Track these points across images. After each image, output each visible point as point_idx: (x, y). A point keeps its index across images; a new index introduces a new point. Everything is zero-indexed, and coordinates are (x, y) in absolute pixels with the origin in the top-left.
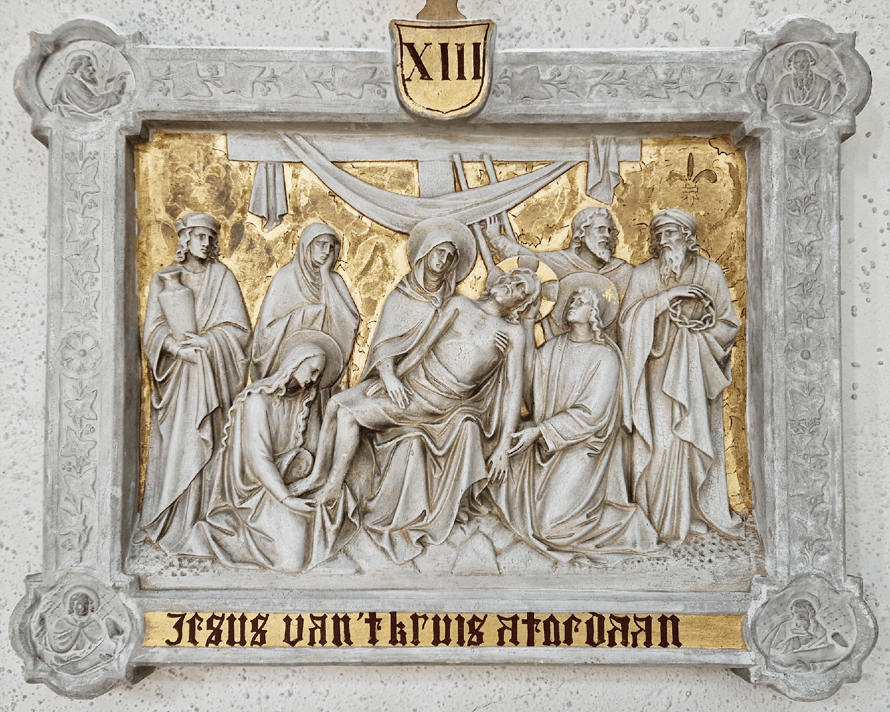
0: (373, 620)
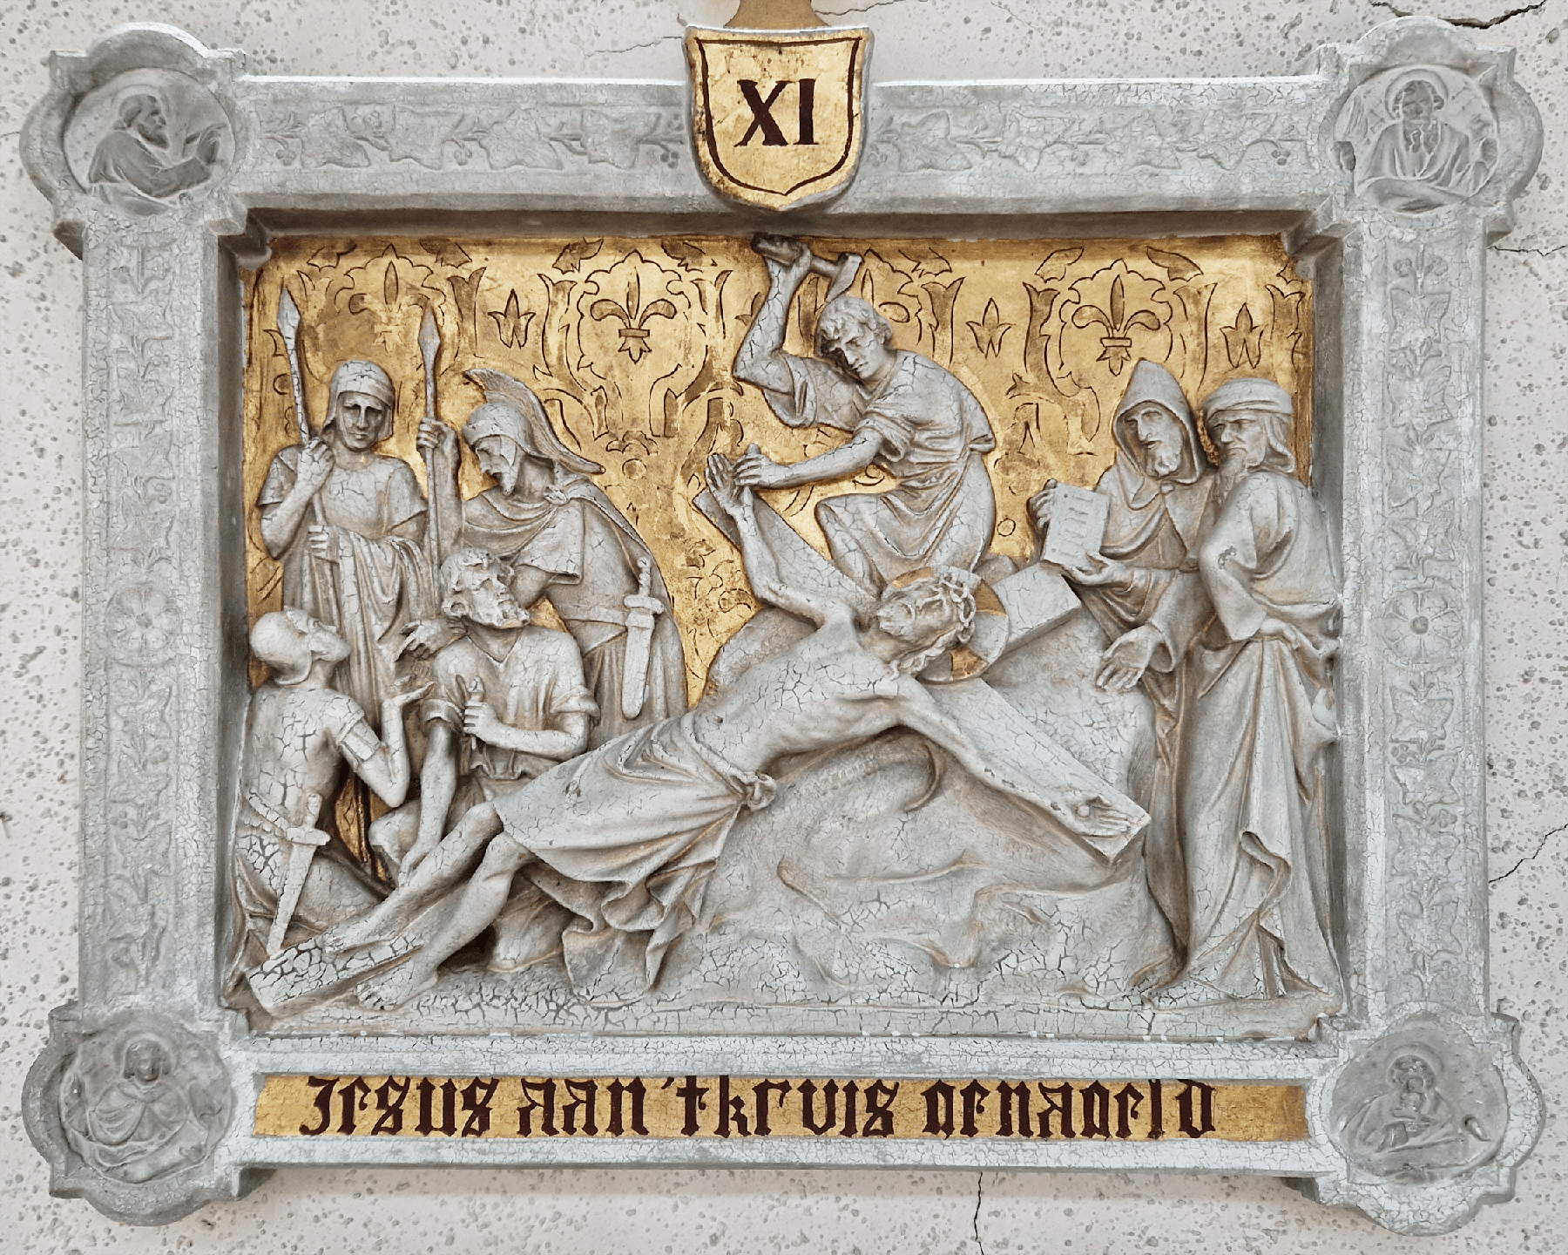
0: (691, 1092)
